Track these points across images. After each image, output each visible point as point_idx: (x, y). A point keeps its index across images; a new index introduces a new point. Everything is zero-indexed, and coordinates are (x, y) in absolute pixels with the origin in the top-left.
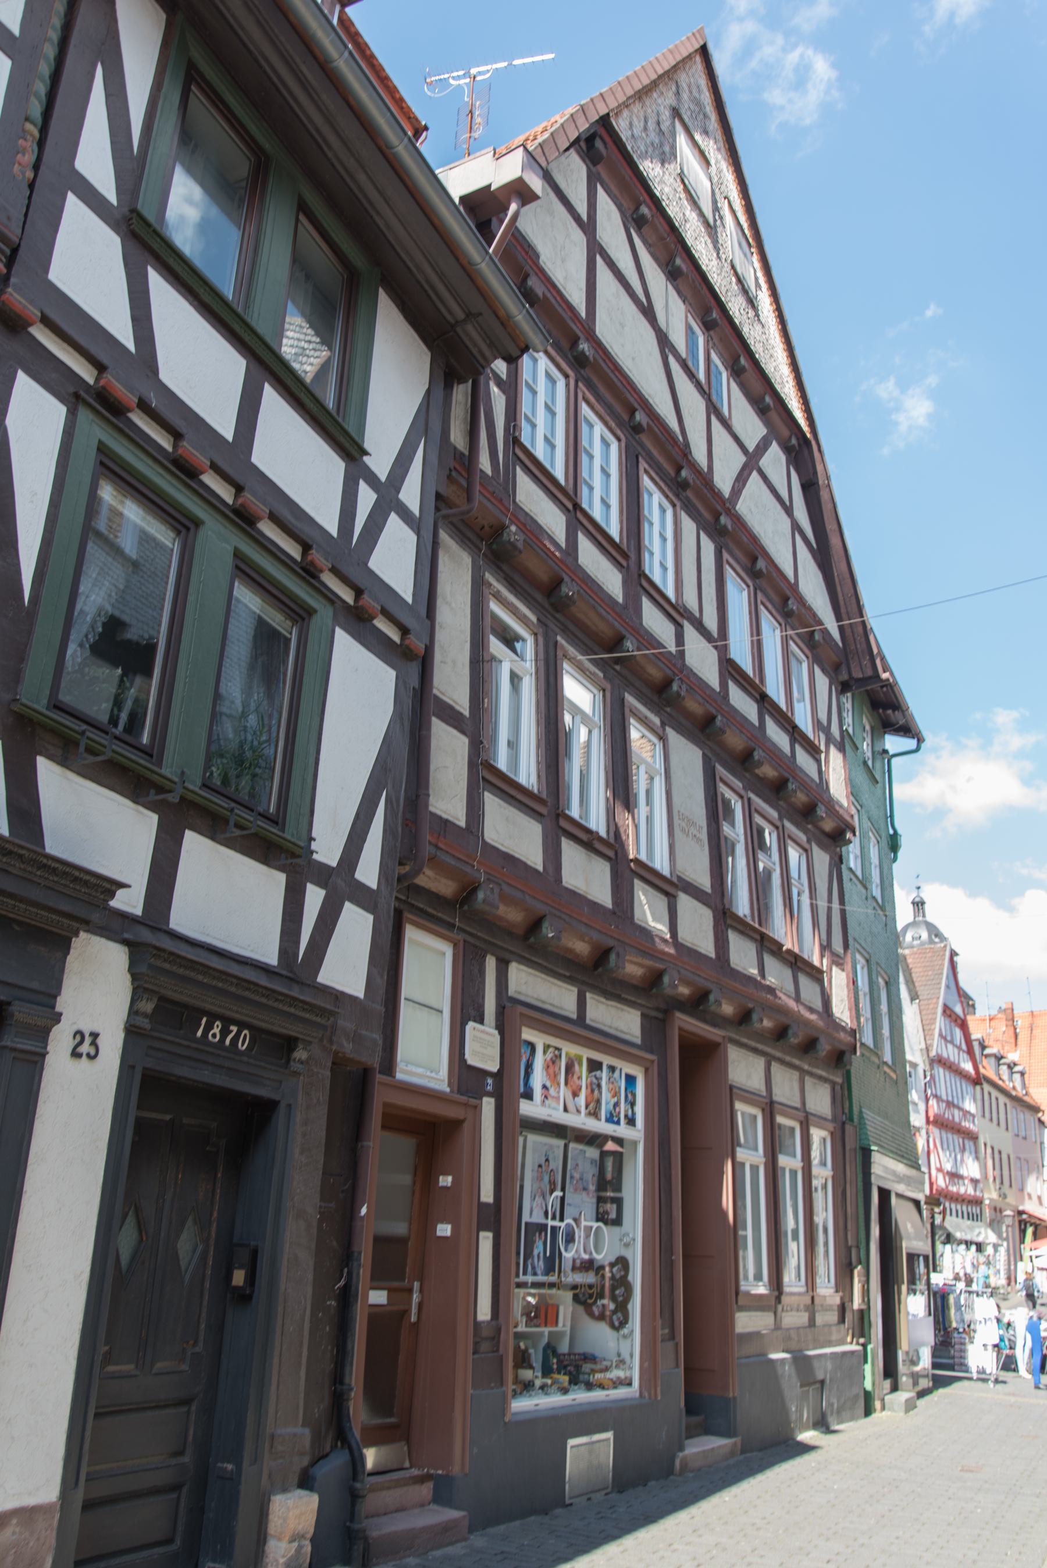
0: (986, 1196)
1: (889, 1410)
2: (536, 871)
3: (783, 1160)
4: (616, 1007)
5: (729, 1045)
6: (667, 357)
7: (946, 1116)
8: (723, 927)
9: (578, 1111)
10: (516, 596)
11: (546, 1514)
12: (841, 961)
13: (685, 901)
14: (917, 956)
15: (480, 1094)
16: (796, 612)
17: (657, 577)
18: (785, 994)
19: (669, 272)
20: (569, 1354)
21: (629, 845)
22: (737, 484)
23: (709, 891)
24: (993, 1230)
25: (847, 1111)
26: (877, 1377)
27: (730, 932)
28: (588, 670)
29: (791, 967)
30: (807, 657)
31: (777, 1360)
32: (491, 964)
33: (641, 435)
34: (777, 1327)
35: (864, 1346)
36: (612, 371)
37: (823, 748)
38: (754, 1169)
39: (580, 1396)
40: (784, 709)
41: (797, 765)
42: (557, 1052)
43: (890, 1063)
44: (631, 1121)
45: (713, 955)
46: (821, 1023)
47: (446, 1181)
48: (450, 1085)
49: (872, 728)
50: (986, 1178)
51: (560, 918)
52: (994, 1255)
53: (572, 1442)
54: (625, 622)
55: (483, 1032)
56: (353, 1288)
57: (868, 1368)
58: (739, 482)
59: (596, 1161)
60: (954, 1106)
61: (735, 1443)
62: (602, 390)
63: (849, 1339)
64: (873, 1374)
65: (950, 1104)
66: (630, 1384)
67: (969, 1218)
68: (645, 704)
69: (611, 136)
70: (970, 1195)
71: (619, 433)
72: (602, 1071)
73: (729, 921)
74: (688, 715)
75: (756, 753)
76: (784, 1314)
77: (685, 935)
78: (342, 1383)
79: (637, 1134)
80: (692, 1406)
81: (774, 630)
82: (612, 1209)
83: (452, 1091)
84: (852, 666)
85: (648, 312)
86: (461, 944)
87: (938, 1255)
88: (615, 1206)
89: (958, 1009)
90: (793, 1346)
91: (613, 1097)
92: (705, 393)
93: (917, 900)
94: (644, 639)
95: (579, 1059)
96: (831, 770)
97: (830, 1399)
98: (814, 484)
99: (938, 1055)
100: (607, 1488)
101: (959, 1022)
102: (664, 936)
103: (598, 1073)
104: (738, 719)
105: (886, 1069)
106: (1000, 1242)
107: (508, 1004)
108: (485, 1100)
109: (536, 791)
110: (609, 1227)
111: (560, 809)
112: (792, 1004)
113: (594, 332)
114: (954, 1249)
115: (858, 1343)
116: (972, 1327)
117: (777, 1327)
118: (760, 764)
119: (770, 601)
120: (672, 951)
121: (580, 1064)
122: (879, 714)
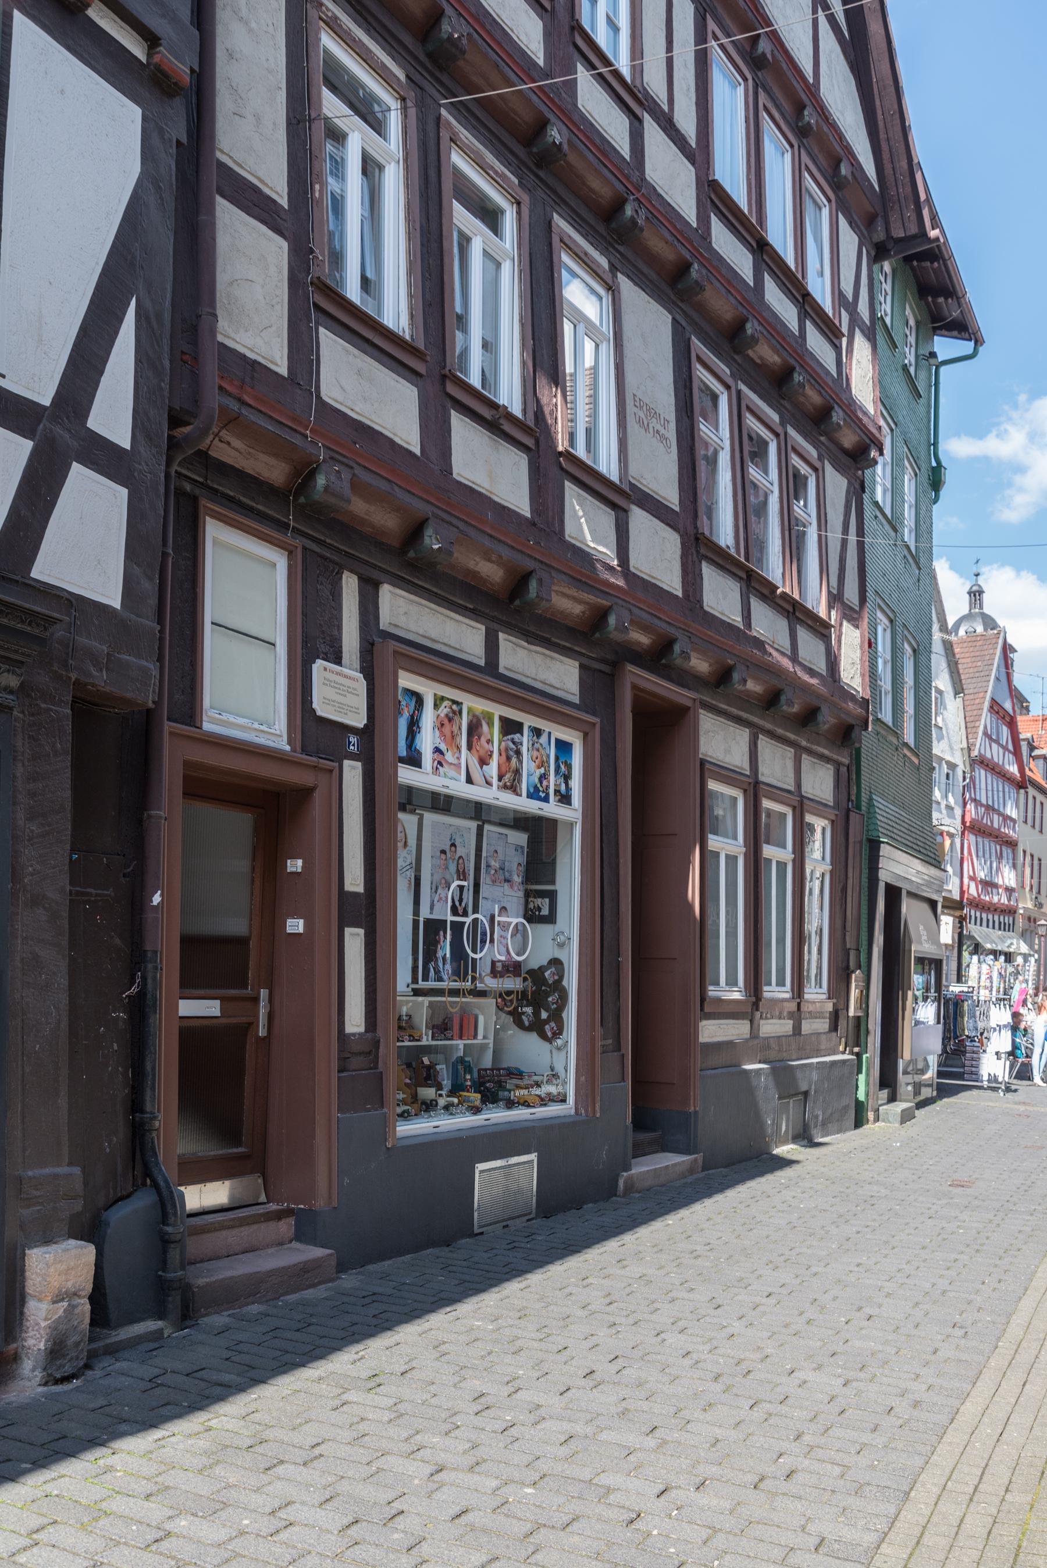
0: (1020, 905)
1: (883, 1121)
2: (410, 453)
3: (769, 851)
4: (544, 654)
5: (701, 711)
7: (985, 821)
8: (695, 558)
9: (489, 783)
10: (368, 32)
11: (448, 1246)
12: (855, 616)
13: (639, 519)
14: (965, 645)
15: (340, 755)
17: (602, 37)
18: (777, 650)
20: (492, 1070)
21: (556, 433)
23: (677, 509)
24: (1025, 942)
25: (853, 798)
26: (871, 1086)
27: (704, 565)
28: (492, 168)
29: (788, 618)
30: (829, 201)
31: (751, 1071)
32: (350, 585)
34: (754, 1034)
35: (859, 1055)
37: (845, 329)
38: (731, 860)
39: (497, 1116)
40: (793, 267)
41: (807, 349)
42: (454, 707)
43: (912, 744)
44: (565, 799)
45: (680, 594)
46: (823, 690)
47: (295, 865)
48: (289, 743)
49: (918, 323)
50: (1023, 887)
51: (450, 524)
52: (1024, 966)
53: (480, 1166)
54: (549, 97)
55: (338, 674)
56: (149, 996)
57: (862, 1078)
59: (522, 847)
60: (994, 810)
61: (696, 1160)
63: (841, 1048)
64: (867, 1084)
65: (989, 808)
66: (564, 1101)
67: (1000, 929)
68: (585, 236)
70: (1003, 904)
72: (522, 735)
73: (703, 551)
74: (652, 259)
75: (748, 326)
76: (762, 1022)
77: (641, 562)
78: (142, 1111)
79: (572, 814)
80: (640, 1123)
81: (783, 154)
82: (544, 904)
83: (293, 750)
84: (892, 220)
86: (299, 551)
87: (964, 965)
88: (547, 900)
89: (1008, 706)
90: (773, 1055)
91: (539, 767)
93: (975, 588)
94: (579, 129)
95: (489, 718)
96: (854, 362)
97: (816, 1111)
99: (980, 754)
100: (530, 1214)
101: (1008, 719)
103: (517, 737)
104: (724, 271)
105: (906, 751)
106: (1032, 953)
107: (378, 640)
108: (347, 763)
109: (407, 337)
110: (533, 925)
111: (447, 369)
112: (786, 663)
114: (982, 960)
115: (852, 1053)
116: (985, 1035)
117: (754, 1034)
118: (754, 341)
119: (778, 107)
120: (621, 583)
121: (490, 724)
122: (927, 304)
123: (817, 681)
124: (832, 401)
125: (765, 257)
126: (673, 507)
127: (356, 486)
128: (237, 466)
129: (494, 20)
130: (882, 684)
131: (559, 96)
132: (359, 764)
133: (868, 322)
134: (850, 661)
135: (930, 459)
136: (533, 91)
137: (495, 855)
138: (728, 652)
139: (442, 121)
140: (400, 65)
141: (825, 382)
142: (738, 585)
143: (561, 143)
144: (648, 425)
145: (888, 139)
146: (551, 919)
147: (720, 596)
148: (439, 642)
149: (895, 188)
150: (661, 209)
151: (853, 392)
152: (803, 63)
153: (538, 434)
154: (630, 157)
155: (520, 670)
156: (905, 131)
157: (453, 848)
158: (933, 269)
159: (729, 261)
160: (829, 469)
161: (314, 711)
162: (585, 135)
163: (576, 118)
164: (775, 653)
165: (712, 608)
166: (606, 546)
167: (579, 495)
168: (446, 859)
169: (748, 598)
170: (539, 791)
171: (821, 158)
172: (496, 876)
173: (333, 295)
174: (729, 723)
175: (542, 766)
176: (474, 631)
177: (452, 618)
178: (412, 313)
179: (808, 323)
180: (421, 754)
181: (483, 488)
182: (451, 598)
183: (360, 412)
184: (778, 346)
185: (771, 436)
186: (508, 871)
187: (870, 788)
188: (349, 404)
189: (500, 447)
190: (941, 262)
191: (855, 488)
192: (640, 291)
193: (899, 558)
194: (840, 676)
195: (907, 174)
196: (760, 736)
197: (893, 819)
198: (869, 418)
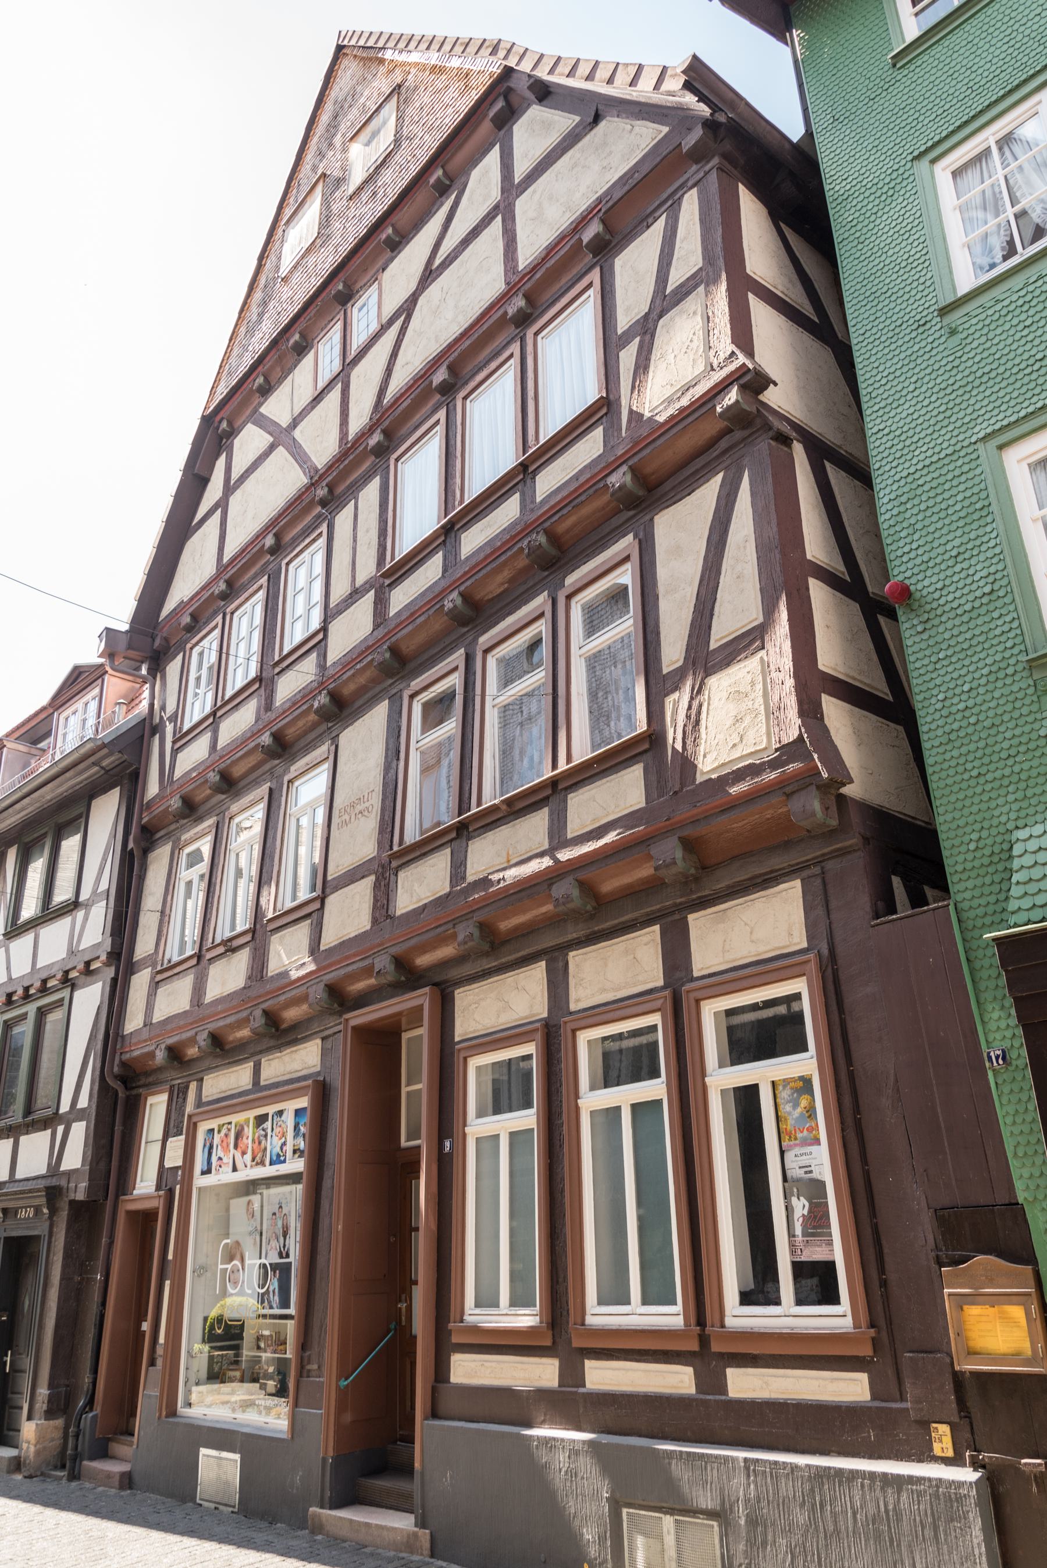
85: (408, 308)
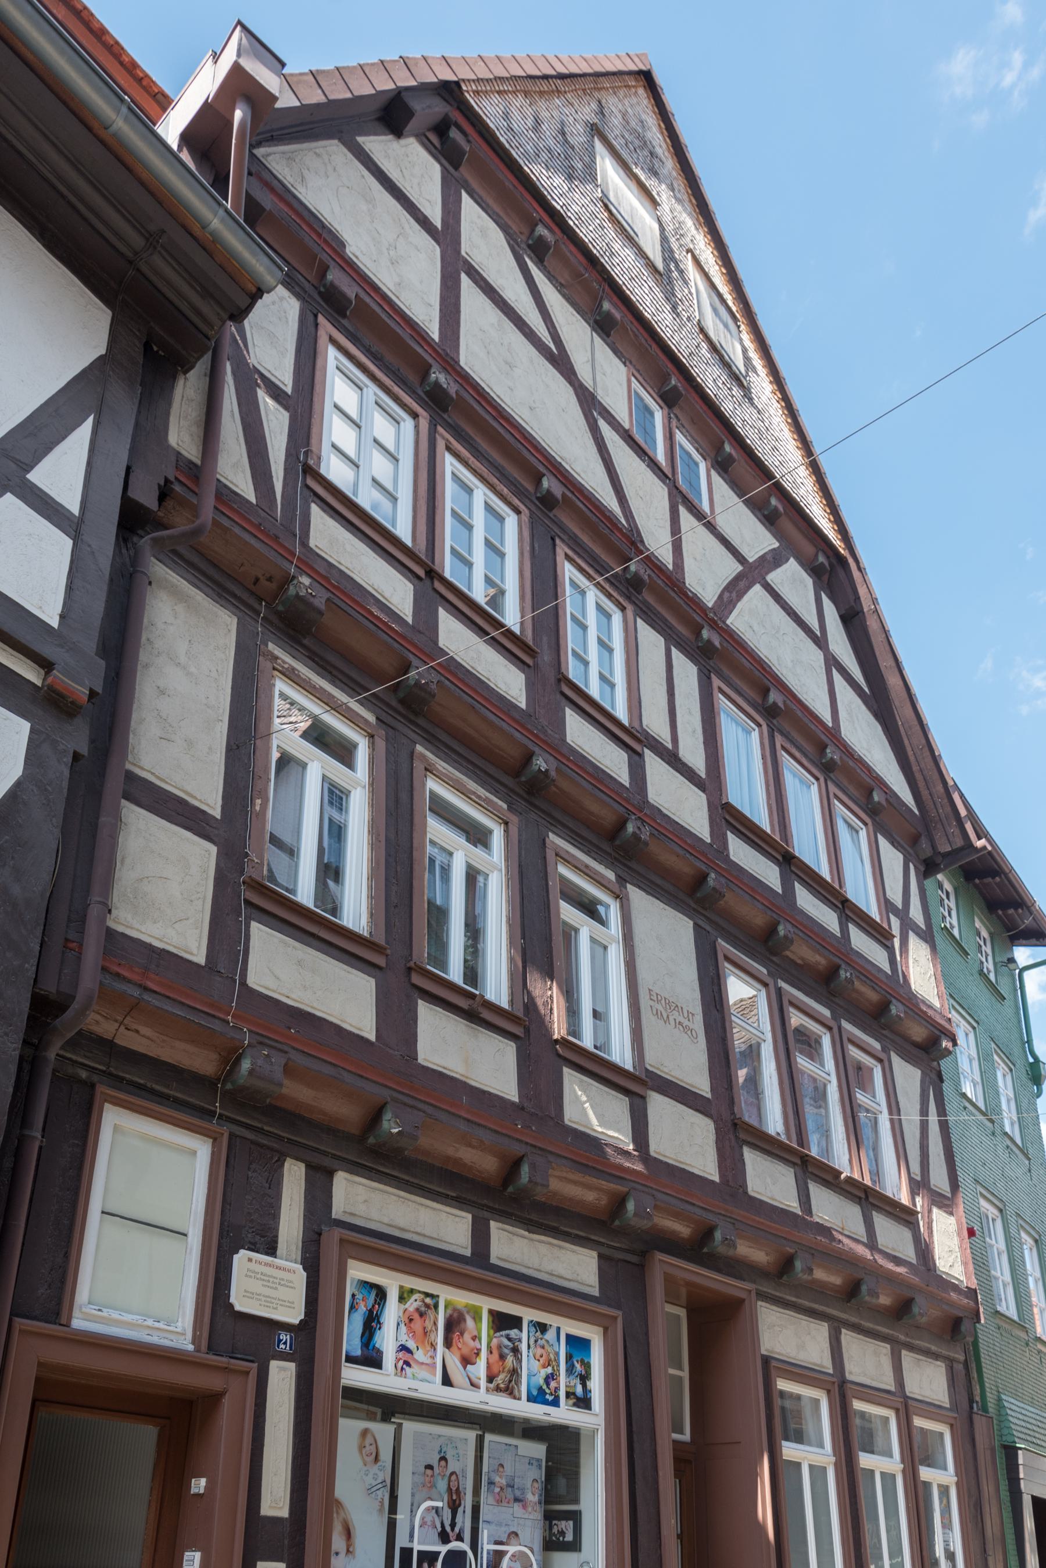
2: (366, 1041)
3: (865, 1460)
6: (596, 421)
9: (474, 1385)
13: (658, 1105)
16: (839, 762)
19: (596, 322)
21: (552, 1022)
22: (726, 595)
23: (709, 1095)
25: (978, 1398)
28: (474, 793)
29: (860, 1204)
30: (865, 824)
33: (555, 511)
36: (495, 418)
41: (852, 949)
42: (428, 1300)
44: (583, 1402)
45: (716, 1178)
46: (915, 1280)
48: (193, 1343)
49: (991, 935)
58: (731, 592)
59: (539, 1460)
62: (483, 445)
68: (588, 853)
69: (473, 125)
71: (516, 502)
72: (521, 1330)
73: (742, 1136)
74: (666, 873)
83: (198, 1350)
84: (937, 837)
88: (571, 1523)
91: (544, 1367)
92: (667, 477)
94: (569, 760)
96: (911, 961)
98: (858, 613)
102: (625, 1148)
103: (513, 1333)
113: (457, 362)
118: (788, 941)
120: (639, 1167)
121: (477, 1317)
122: (999, 917)
123: (906, 1270)
124: (888, 996)
125: (793, 868)
126: (704, 1094)
127: (289, 1070)
128: (151, 1054)
129: (468, 671)
130: (999, 1274)
131: (545, 732)
132: (292, 1366)
133: (923, 927)
134: (946, 1249)
135: (1026, 1056)
136: (435, 669)
137: (501, 1469)
138: (785, 1239)
139: (415, 754)
140: (369, 710)
141: (877, 978)
142: (792, 1170)
143: (547, 770)
144: (668, 1017)
145: (921, 770)
146: (575, 1546)
147: (769, 1180)
148: (410, 1231)
149: (935, 811)
150: (668, 827)
151: (913, 987)
152: (820, 710)
153: (527, 1023)
154: (630, 784)
155: (519, 1260)
156: (936, 760)
157: (443, 1463)
158: (996, 884)
159: (751, 871)
160: (896, 1060)
161: (232, 1306)
162: (576, 765)
163: (565, 751)
164: (845, 1240)
165: (758, 1193)
166: (618, 1131)
167: (582, 1081)
168: (432, 1476)
169: (806, 1185)
170: (546, 1393)
171: (851, 789)
172: (502, 1494)
173: (267, 892)
174: (800, 1316)
175: (549, 1365)
176: (457, 1219)
177: (427, 1206)
178: (372, 913)
179: (851, 926)
180: (382, 1353)
181: (457, 1073)
182: (428, 1186)
183: (298, 999)
184: (818, 946)
185: (824, 1030)
186: (518, 1489)
187: (997, 1387)
188: (285, 991)
189: (480, 1034)
190: (1003, 876)
191: (930, 1078)
192: (654, 899)
193: (1000, 1149)
194: (935, 1264)
195: (945, 796)
196: (843, 1331)
197: (1034, 1422)
198: (935, 1010)
